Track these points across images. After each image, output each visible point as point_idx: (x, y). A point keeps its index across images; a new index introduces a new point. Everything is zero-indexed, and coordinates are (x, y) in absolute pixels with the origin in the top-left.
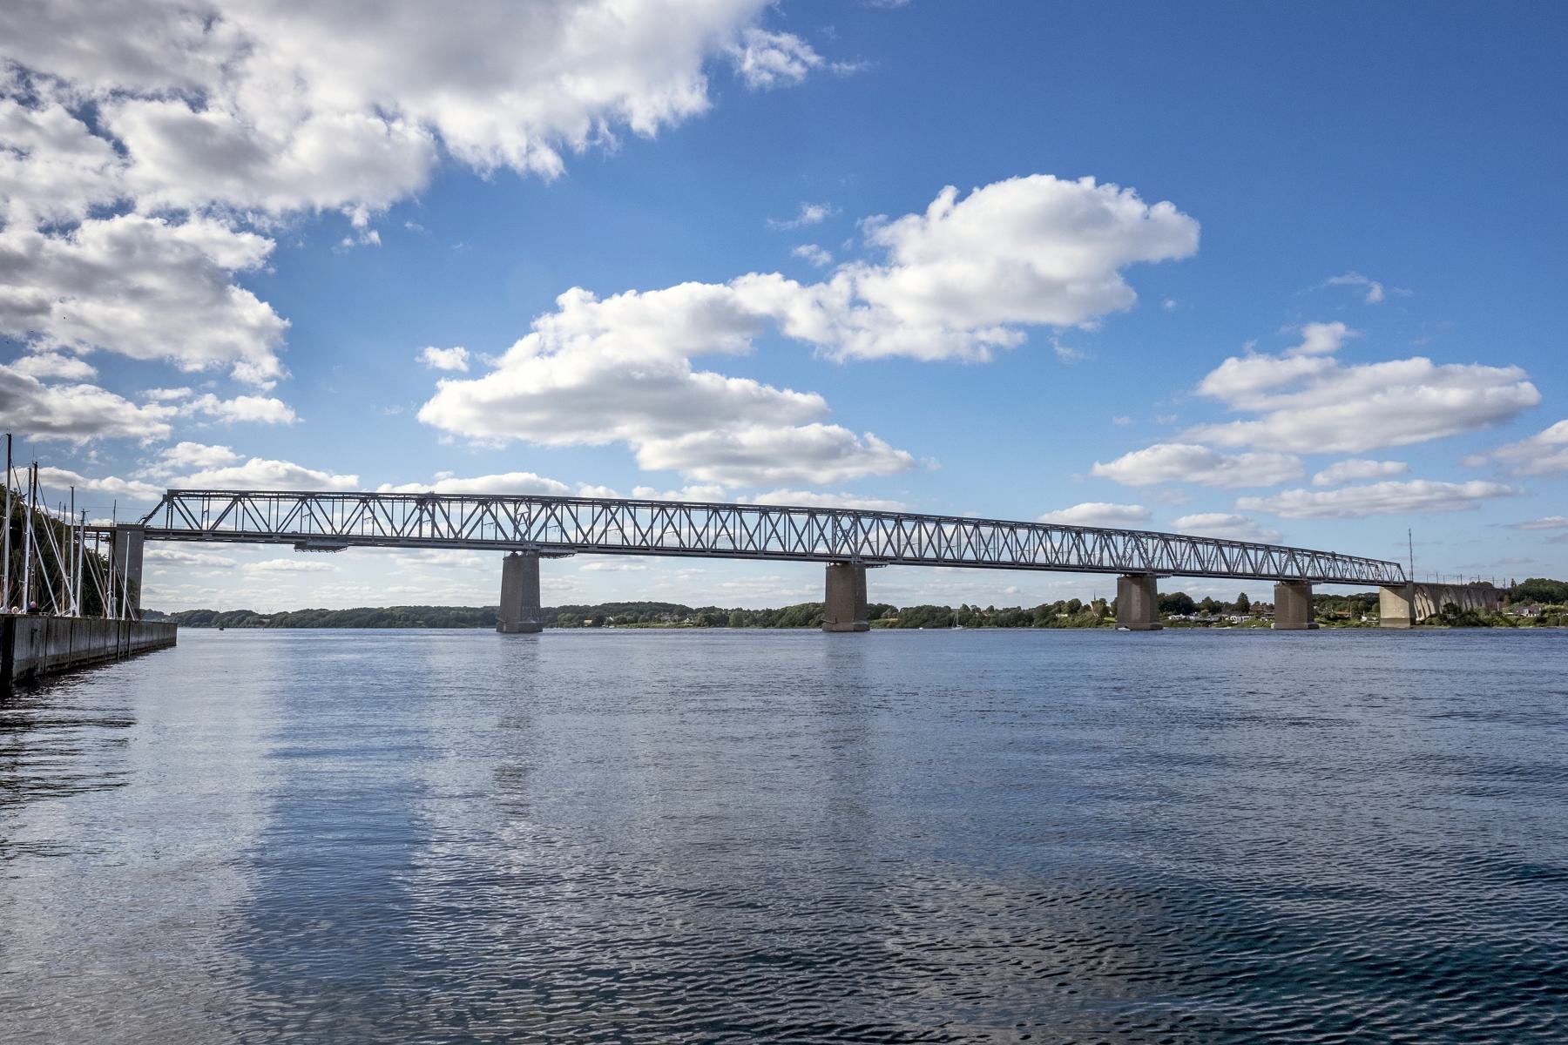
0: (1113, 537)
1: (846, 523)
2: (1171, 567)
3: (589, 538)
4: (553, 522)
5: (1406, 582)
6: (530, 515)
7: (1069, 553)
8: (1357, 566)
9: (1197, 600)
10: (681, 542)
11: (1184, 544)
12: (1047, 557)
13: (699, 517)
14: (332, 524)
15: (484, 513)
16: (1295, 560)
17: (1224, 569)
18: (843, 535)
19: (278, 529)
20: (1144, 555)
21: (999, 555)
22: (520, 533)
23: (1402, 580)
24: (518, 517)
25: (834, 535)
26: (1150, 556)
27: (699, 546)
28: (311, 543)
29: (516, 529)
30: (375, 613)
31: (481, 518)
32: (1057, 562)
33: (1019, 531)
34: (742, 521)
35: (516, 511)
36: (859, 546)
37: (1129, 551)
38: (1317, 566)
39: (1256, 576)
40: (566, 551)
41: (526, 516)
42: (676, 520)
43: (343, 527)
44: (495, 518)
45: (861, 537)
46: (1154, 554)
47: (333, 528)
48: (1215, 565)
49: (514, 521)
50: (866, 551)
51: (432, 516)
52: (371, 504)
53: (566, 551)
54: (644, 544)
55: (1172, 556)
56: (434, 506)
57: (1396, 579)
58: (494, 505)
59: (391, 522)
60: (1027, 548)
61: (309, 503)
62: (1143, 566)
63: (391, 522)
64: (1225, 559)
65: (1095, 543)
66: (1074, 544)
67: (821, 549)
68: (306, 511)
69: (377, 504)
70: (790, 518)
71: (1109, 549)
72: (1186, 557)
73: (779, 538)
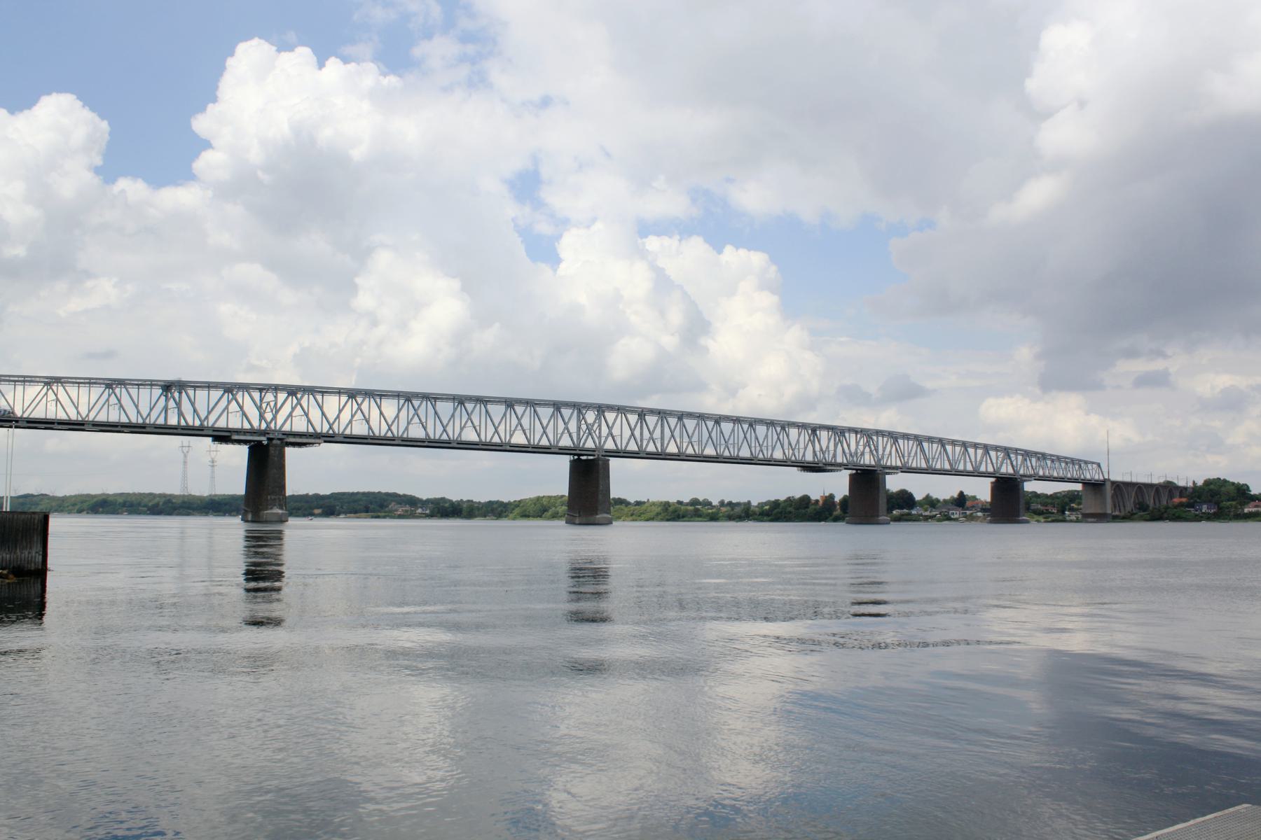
0: (847, 435)
1: (590, 416)
2: (899, 464)
3: (394, 428)
4: (298, 411)
5: (1105, 480)
6: (276, 404)
7: (805, 448)
8: (1063, 465)
9: (919, 496)
10: (370, 428)
11: (911, 442)
12: (784, 453)
13: (445, 408)
14: (77, 408)
15: (229, 402)
16: (1010, 459)
17: (947, 467)
18: (587, 428)
19: (23, 412)
20: (874, 452)
21: (739, 450)
22: (266, 421)
23: (1101, 478)
24: (264, 406)
25: (579, 428)
26: (880, 452)
27: (445, 437)
28: (235, 437)
29: (262, 417)
30: (101, 498)
31: (227, 408)
32: (793, 458)
33: (723, 425)
34: (487, 411)
35: (261, 400)
36: (603, 439)
37: (861, 448)
38: (1029, 465)
39: (976, 473)
40: (835, 468)
41: (272, 404)
42: (422, 412)
43: (89, 411)
44: (241, 408)
45: (605, 430)
46: (884, 451)
47: (78, 413)
48: (939, 462)
49: (259, 408)
50: (610, 445)
51: (179, 405)
52: (117, 391)
53: (835, 468)
54: (389, 434)
55: (900, 455)
56: (180, 393)
57: (1097, 477)
58: (241, 393)
59: (137, 407)
60: (765, 444)
61: (305, 404)
62: (873, 463)
63: (137, 407)
64: (948, 457)
65: (829, 440)
66: (810, 440)
67: (565, 442)
68: (51, 396)
69: (124, 390)
70: (535, 411)
71: (842, 446)
72: (912, 454)
73: (475, 427)
